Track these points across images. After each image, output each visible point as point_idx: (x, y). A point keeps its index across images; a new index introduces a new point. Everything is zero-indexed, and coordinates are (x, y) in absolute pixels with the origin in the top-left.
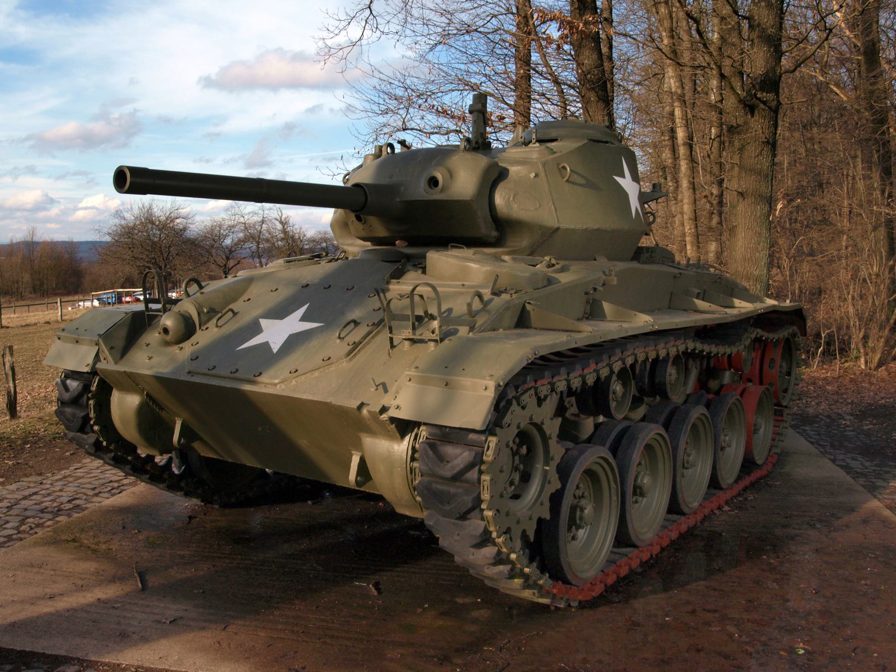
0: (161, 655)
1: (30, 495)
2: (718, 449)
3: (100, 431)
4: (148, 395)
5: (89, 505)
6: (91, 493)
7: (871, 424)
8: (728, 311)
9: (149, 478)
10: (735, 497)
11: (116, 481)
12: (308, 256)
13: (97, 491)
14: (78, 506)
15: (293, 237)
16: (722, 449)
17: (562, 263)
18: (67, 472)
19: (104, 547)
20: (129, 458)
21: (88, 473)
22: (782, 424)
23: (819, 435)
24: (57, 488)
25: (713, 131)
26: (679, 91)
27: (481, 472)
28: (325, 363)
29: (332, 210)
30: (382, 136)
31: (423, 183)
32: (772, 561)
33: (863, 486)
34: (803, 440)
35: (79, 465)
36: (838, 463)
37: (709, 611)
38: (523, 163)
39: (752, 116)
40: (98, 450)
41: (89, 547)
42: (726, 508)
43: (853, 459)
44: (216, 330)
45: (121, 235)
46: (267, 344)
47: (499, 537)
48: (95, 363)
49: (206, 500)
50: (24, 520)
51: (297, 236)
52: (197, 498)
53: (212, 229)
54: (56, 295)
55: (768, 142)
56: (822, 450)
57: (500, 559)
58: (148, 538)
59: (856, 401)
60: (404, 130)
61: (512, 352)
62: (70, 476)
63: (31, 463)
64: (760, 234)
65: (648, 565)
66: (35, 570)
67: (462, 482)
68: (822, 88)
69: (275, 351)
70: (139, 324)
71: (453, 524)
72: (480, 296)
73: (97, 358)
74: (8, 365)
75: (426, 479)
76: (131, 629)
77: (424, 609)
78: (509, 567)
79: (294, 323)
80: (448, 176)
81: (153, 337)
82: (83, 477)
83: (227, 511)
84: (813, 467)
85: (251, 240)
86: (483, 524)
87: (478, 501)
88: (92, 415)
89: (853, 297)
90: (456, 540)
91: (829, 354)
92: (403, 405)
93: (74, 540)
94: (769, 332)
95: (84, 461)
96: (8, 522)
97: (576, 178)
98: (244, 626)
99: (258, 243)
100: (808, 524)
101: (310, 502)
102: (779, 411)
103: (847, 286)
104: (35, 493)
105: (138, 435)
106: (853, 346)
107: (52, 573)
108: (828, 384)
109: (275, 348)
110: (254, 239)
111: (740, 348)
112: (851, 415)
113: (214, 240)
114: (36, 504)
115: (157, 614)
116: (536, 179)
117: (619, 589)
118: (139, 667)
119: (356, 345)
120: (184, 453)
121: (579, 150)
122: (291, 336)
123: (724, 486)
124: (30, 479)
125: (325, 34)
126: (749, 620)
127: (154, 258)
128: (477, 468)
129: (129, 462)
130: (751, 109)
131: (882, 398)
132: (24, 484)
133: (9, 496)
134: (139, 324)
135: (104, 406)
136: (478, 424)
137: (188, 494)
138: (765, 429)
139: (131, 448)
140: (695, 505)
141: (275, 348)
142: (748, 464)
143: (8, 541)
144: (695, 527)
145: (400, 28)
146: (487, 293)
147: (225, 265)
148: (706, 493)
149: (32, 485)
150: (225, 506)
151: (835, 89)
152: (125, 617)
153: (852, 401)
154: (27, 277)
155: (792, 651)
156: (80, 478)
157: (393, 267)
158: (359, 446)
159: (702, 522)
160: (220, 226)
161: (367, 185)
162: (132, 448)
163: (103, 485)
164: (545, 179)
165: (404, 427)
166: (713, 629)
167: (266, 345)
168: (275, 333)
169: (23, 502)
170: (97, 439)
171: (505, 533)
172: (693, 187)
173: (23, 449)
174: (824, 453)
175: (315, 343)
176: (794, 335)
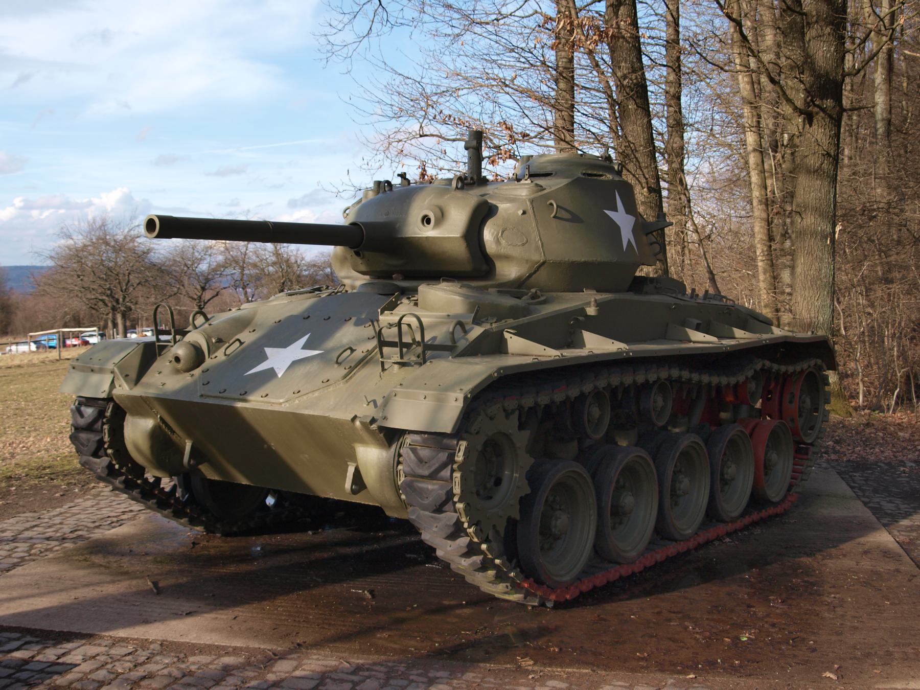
2: (720, 482)
3: (113, 454)
4: (161, 418)
8: (725, 342)
12: (308, 289)
13: (97, 524)
15: (288, 261)
18: (62, 510)
20: (139, 482)
27: (453, 471)
28: (325, 385)
30: (395, 144)
35: (72, 504)
37: (674, 612)
39: (811, 126)
40: (111, 472)
45: (69, 258)
46: (272, 369)
49: (209, 530)
51: (293, 260)
57: (472, 550)
60: (421, 136)
61: (480, 369)
62: (65, 512)
64: (821, 259)
75: (409, 478)
77: (413, 608)
78: (481, 557)
83: (229, 539)
86: (456, 515)
88: (106, 439)
95: (77, 501)
99: (243, 268)
101: (310, 533)
104: (36, 526)
108: (901, 430)
113: (186, 265)
125: (328, 30)
127: (109, 289)
129: (138, 486)
130: (809, 118)
136: (448, 429)
137: (193, 522)
138: (783, 465)
139: (139, 471)
142: (757, 500)
144: (689, 551)
147: (200, 297)
150: (227, 534)
158: (353, 457)
159: (696, 549)
161: (362, 223)
163: (102, 519)
164: (532, 215)
170: (110, 463)
174: (858, 497)
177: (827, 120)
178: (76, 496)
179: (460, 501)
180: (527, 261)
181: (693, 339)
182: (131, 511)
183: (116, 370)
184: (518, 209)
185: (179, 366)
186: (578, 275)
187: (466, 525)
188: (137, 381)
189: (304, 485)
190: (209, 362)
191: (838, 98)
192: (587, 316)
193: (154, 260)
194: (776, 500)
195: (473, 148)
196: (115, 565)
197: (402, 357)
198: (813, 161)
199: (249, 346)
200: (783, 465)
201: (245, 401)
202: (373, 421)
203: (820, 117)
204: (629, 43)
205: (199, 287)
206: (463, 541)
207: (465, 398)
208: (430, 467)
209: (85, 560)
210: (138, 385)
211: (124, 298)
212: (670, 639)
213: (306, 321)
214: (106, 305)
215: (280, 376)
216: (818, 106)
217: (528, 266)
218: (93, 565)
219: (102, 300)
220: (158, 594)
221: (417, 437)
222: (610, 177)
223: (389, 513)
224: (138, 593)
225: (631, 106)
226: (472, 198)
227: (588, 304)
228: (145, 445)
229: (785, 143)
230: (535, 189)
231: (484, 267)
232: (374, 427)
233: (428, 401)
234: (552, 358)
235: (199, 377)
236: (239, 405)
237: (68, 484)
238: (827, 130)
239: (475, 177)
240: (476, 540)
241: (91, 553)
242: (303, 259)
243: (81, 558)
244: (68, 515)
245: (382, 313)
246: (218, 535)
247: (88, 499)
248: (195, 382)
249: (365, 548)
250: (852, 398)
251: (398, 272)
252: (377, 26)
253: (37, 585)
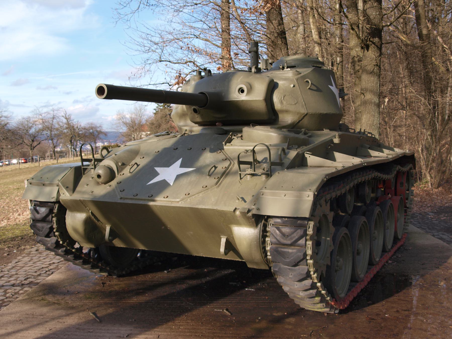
3: (59, 235)
4: (91, 212)
7: (444, 216)
13: (38, 273)
15: (73, 127)
22: (408, 217)
23: (420, 223)
27: (306, 240)
35: (17, 260)
39: (368, 51)
42: (390, 262)
43: (443, 234)
47: (314, 274)
51: (75, 127)
55: (377, 65)
59: (432, 205)
67: (295, 246)
71: (289, 269)
83: (121, 279)
85: (47, 129)
86: (306, 267)
87: (305, 255)
88: (55, 226)
99: (51, 131)
101: (166, 272)
112: (432, 212)
128: (304, 238)
131: (446, 203)
140: (377, 260)
144: (378, 272)
147: (31, 145)
148: (382, 254)
150: (119, 276)
153: (431, 206)
163: (39, 269)
164: (298, 88)
174: (427, 232)
176: (411, 169)
177: (376, 48)
178: (17, 255)
180: (298, 113)
181: (372, 155)
182: (54, 263)
183: (60, 184)
185: (100, 180)
188: (74, 190)
189: (185, 249)
190: (119, 178)
191: (380, 37)
193: (10, 128)
196: (63, 301)
198: (370, 68)
199: (144, 167)
201: (154, 201)
202: (249, 211)
203: (372, 48)
204: (277, 11)
205: (31, 140)
206: (308, 282)
207: (314, 194)
208: (291, 239)
209: (43, 299)
210: (75, 193)
213: (177, 151)
215: (172, 185)
216: (371, 41)
217: (298, 116)
218: (49, 304)
220: (101, 322)
221: (279, 220)
223: (249, 266)
224: (88, 322)
225: (280, 42)
228: (80, 228)
229: (338, 62)
231: (274, 117)
232: (250, 214)
233: (289, 198)
235: (116, 187)
236: (151, 203)
237: (9, 247)
238: (376, 53)
241: (44, 294)
242: (80, 126)
243: (40, 298)
244: (18, 268)
245: (225, 144)
246: (115, 277)
247: (24, 257)
248: (114, 190)
249: (204, 280)
250: (426, 184)
251: (219, 122)
252: (142, 6)
253: (20, 321)
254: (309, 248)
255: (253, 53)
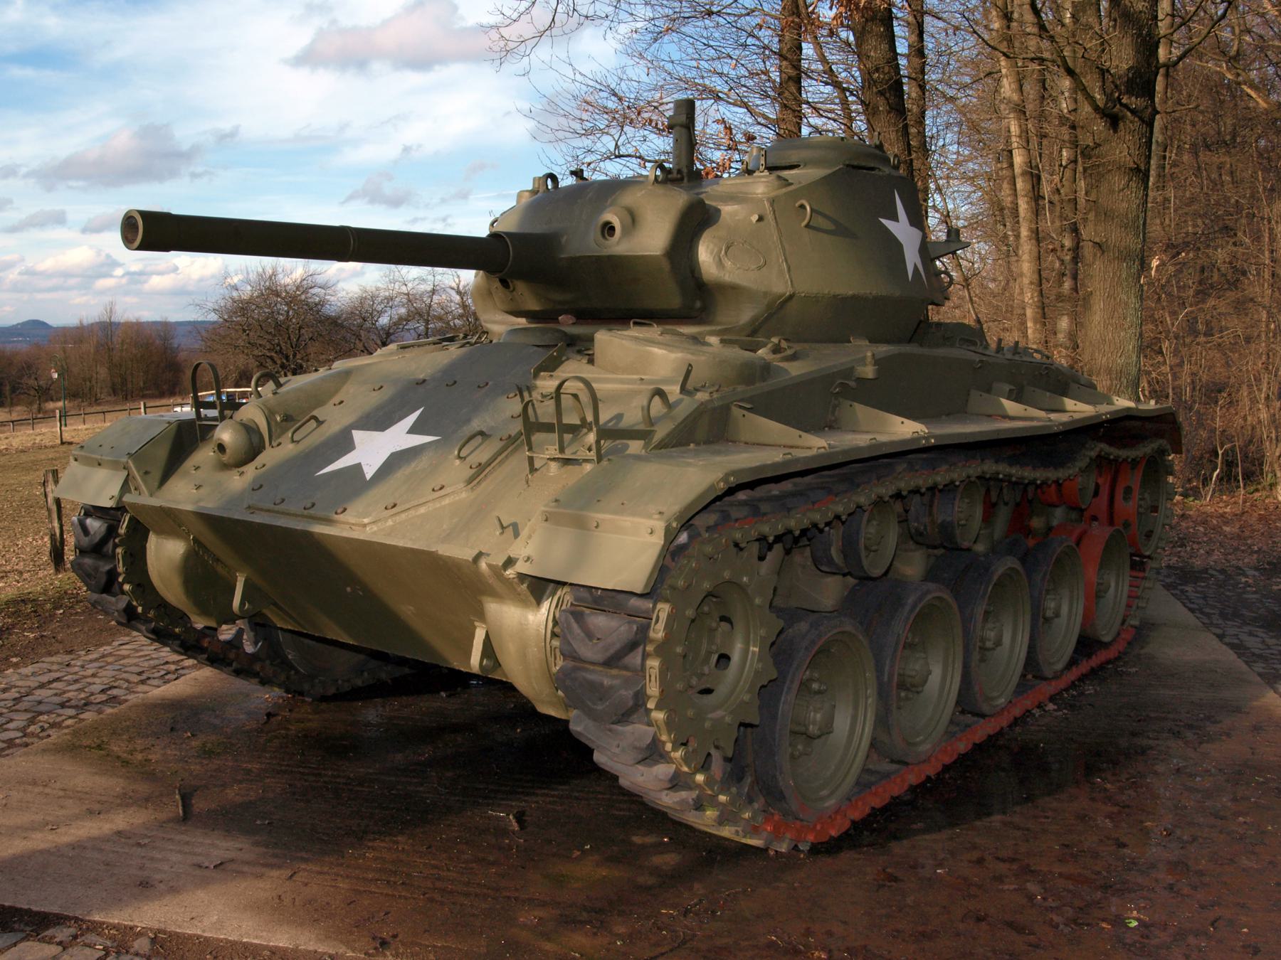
0: (194, 914)
1: (50, 682)
2: (1040, 622)
3: (133, 591)
4: (196, 540)
5: (129, 697)
6: (136, 679)
8: (1053, 416)
9: (208, 659)
10: (1066, 690)
11: (173, 663)
13: (144, 677)
14: (115, 697)
16: (1047, 620)
17: (797, 347)
19: (140, 757)
21: (136, 651)
23: (1205, 598)
24: (90, 672)
25: (1064, 153)
26: (1015, 97)
27: (645, 656)
29: (473, 272)
31: (595, 233)
32: (1108, 786)
33: (1260, 675)
34: (1179, 605)
36: (1227, 640)
37: (1003, 860)
38: (744, 199)
39: (1115, 131)
40: (130, 618)
41: (118, 757)
42: (1051, 707)
43: (1251, 634)
44: (291, 446)
48: (121, 496)
50: (34, 717)
52: (279, 686)
53: (362, 300)
54: (144, 397)
55: (1138, 169)
56: (1206, 621)
58: (204, 744)
59: (1265, 548)
61: (697, 475)
62: (110, 654)
63: (60, 637)
65: (925, 789)
66: (37, 790)
68: (1234, 87)
69: (368, 477)
70: (185, 440)
72: (660, 393)
73: (125, 488)
74: (50, 499)
76: (158, 877)
77: (584, 852)
79: (399, 437)
80: (629, 220)
81: (204, 455)
82: (128, 656)
84: (1189, 644)
86: (651, 730)
88: (121, 569)
89: (1267, 398)
90: (614, 752)
91: (1228, 478)
92: (532, 551)
93: (99, 747)
94: (1119, 448)
96: (12, 720)
97: (820, 222)
98: (320, 873)
99: (427, 322)
100: (1170, 731)
101: (443, 694)
102: (1138, 564)
103: (1258, 380)
105: (183, 598)
106: (1266, 468)
107: (61, 793)
108: (1226, 523)
109: (369, 472)
110: (420, 315)
111: (1075, 473)
112: (1256, 569)
114: (56, 695)
115: (200, 855)
116: (761, 224)
117: (878, 827)
118: (160, 931)
119: (481, 468)
120: (260, 625)
121: (826, 180)
122: (392, 454)
123: (1048, 673)
124: (54, 659)
126: (1061, 875)
127: (278, 345)
128: (640, 649)
129: (176, 637)
130: (1114, 121)
132: (45, 665)
133: (20, 683)
134: (185, 440)
135: (137, 557)
136: (639, 589)
137: (264, 682)
140: (1002, 701)
141: (369, 472)
142: (1087, 644)
143: (9, 748)
144: (1001, 733)
145: (610, 10)
146: (673, 390)
149: (55, 667)
151: (1249, 91)
152: (152, 859)
154: (103, 372)
155: (1119, 921)
156: (124, 657)
157: (543, 355)
158: (481, 616)
160: (373, 297)
161: (507, 234)
162: (182, 617)
163: (154, 667)
164: (773, 223)
165: (539, 587)
166: (1006, 887)
167: (358, 468)
168: (371, 451)
169: (38, 692)
170: (129, 604)
171: (683, 744)
172: (1037, 236)
173: (53, 616)
174: (1207, 626)
175: (423, 462)
179: (659, 707)
184: (752, 214)
186: (842, 318)
187: (669, 747)
192: (861, 380)
194: (1107, 639)
195: (682, 126)
197: (562, 450)
200: (1117, 587)
201: (328, 521)
203: (1131, 123)
211: (295, 356)
212: (1011, 925)
214: (275, 362)
219: (271, 358)
222: (887, 170)
226: (679, 199)
227: (862, 361)
230: (777, 183)
234: (814, 452)
239: (685, 170)
240: (685, 769)
251: (566, 312)
254: (653, 678)
255: (677, 128)
